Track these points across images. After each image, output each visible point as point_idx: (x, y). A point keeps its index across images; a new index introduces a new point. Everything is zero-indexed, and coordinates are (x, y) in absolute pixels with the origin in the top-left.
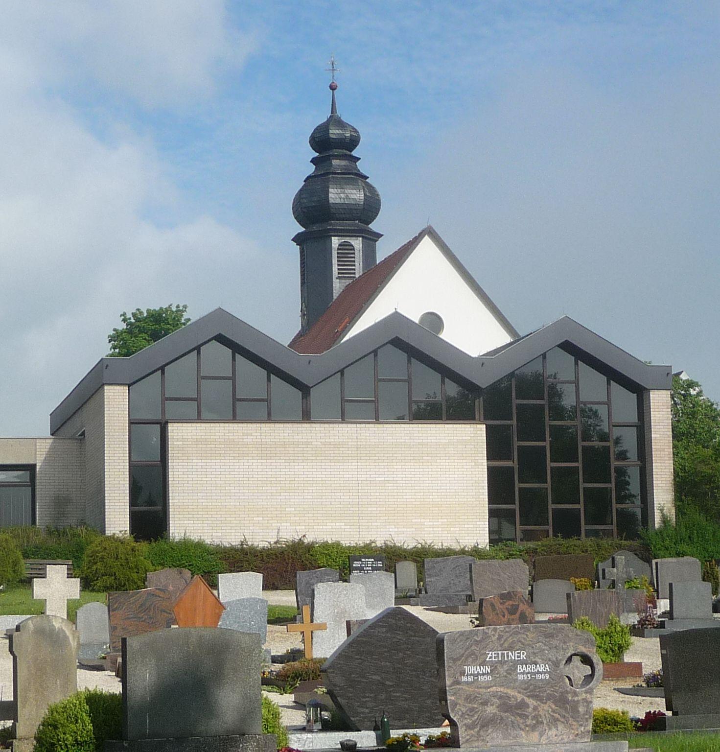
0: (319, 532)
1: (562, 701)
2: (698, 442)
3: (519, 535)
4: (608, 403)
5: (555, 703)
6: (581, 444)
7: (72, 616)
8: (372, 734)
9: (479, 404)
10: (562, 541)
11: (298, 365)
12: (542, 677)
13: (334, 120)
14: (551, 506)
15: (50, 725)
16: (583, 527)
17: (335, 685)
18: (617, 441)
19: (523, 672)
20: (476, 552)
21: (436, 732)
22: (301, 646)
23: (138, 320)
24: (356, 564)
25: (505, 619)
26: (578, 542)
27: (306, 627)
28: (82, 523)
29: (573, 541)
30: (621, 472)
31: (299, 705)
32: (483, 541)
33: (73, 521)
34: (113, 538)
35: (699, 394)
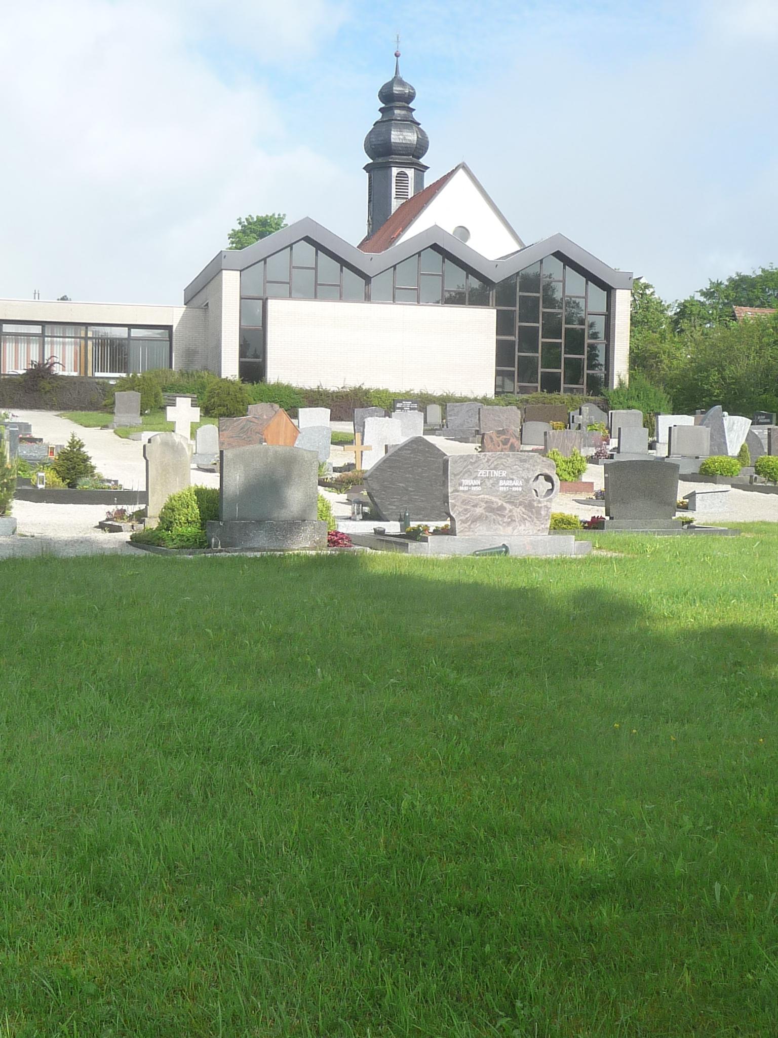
0: (372, 382)
1: (529, 506)
2: (649, 329)
3: (517, 390)
4: (586, 298)
5: (525, 507)
6: (564, 326)
7: (193, 435)
8: (398, 524)
9: (492, 294)
10: (546, 395)
11: (370, 262)
12: (517, 489)
13: (397, 80)
14: (540, 370)
15: (170, 508)
16: (562, 385)
17: (373, 489)
18: (592, 325)
19: (503, 487)
20: (485, 401)
21: (441, 524)
22: (353, 461)
23: (249, 223)
24: (399, 405)
25: (499, 448)
26: (558, 396)
27: (357, 446)
28: (205, 368)
29: (554, 395)
30: (592, 347)
31: (349, 502)
32: (490, 393)
33: (197, 367)
34: (226, 380)
35: (652, 294)
